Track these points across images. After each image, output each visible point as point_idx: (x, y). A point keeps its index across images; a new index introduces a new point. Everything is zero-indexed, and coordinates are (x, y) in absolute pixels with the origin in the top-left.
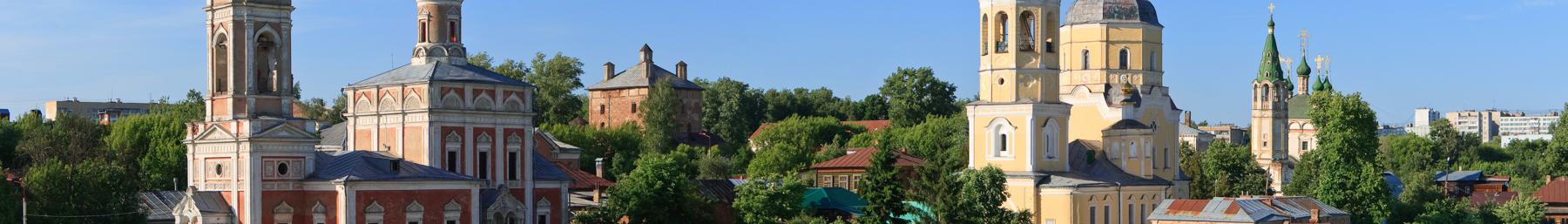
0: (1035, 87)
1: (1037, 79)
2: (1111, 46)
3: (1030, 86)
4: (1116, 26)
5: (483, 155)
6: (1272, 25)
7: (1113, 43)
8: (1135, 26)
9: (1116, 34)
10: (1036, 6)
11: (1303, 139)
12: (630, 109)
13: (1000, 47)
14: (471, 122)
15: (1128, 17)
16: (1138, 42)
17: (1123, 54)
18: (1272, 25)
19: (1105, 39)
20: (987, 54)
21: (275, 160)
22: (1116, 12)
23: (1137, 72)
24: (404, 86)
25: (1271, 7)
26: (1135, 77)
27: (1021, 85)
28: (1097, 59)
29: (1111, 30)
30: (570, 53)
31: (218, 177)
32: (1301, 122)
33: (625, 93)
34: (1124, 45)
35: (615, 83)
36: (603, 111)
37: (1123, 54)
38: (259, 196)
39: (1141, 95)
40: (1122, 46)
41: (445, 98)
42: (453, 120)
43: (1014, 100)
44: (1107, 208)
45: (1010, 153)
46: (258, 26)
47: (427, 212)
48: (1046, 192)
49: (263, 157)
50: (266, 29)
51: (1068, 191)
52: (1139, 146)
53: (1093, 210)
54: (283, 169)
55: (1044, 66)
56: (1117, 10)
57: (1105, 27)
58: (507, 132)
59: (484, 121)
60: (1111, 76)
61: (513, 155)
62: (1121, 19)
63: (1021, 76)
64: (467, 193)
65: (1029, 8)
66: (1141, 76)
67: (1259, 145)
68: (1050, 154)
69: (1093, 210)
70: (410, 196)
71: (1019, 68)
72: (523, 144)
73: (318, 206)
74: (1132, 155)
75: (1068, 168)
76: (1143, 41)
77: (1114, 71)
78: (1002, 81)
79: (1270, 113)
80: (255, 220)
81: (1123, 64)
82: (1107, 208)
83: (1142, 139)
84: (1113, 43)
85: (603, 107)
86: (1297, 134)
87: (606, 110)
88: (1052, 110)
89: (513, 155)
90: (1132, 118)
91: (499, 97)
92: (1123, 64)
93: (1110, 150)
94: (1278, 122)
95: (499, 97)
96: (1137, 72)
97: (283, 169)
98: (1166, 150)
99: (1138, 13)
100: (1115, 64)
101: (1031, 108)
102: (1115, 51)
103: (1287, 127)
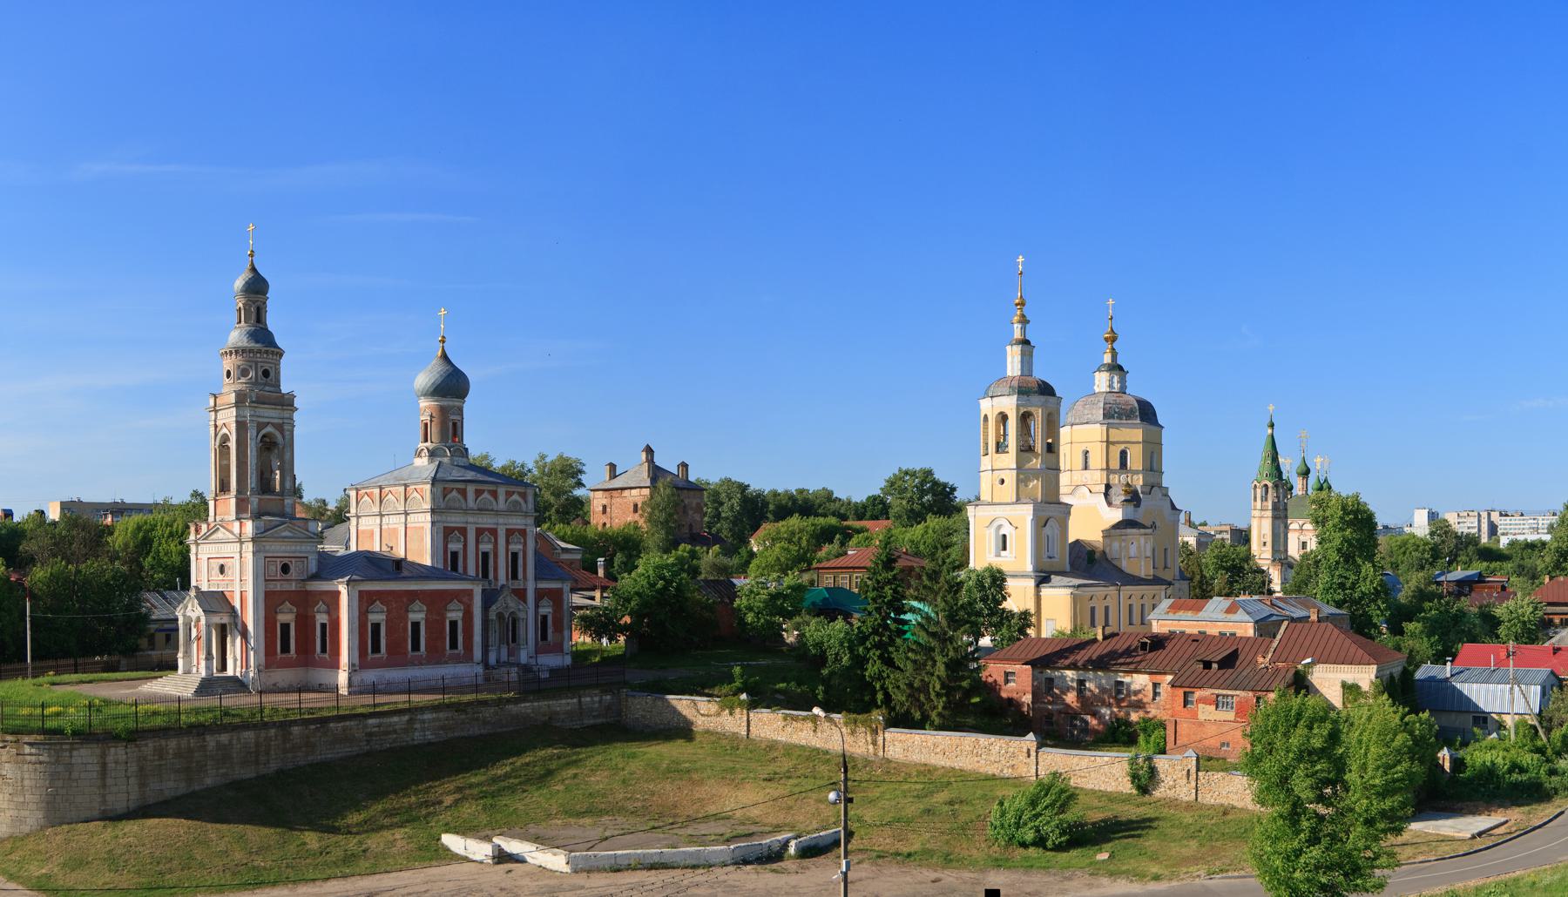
0: (1035, 487)
1: (1038, 480)
2: (1111, 446)
3: (1030, 486)
4: (1117, 427)
5: (485, 555)
6: (1272, 426)
7: (1114, 443)
8: (1134, 426)
9: (1116, 435)
10: (1036, 406)
11: (1303, 539)
12: (632, 509)
13: (1000, 447)
14: (473, 522)
15: (1128, 417)
16: (1138, 443)
17: (1123, 454)
18: (1272, 426)
19: (1105, 439)
20: (987, 454)
21: (278, 560)
22: (1116, 412)
23: (1137, 472)
24: (406, 486)
25: (1271, 408)
26: (1135, 477)
27: (1022, 486)
28: (1097, 460)
29: (1111, 430)
30: (572, 453)
31: (221, 577)
32: (1301, 522)
33: (626, 493)
34: (1125, 445)
35: (617, 483)
36: (604, 511)
37: (1123, 454)
38: (262, 596)
39: (1141, 495)
40: (1122, 447)
41: (446, 499)
42: (455, 520)
43: (1014, 500)
44: (1107, 608)
45: (1011, 553)
46: (260, 426)
47: (429, 612)
48: (1046, 591)
49: (265, 557)
50: (269, 429)
51: (1069, 591)
52: (1139, 547)
53: (1093, 609)
54: (285, 569)
55: (1044, 466)
56: (1117, 410)
57: (1105, 427)
58: (510, 533)
59: (486, 521)
60: (1111, 477)
61: (515, 555)
62: (1121, 419)
63: (1022, 476)
64: (470, 593)
65: (1029, 409)
66: (1141, 476)
67: (1259, 545)
68: (1050, 554)
69: (1093, 609)
70: (413, 596)
71: (1020, 468)
72: (525, 544)
73: (321, 606)
74: (1132, 554)
75: (1068, 568)
76: (1143, 441)
77: (1114, 472)
78: (1002, 482)
79: (1269, 513)
80: (258, 620)
81: (1123, 464)
82: (1107, 608)
83: (1142, 540)
84: (1114, 443)
85: (605, 507)
86: (1297, 534)
87: (608, 510)
88: (1052, 510)
89: (515, 555)
90: (1132, 518)
91: (502, 497)
92: (1123, 464)
93: (1110, 549)
94: (1277, 522)
95: (502, 497)
96: (1137, 472)
97: (285, 569)
98: (1165, 549)
99: (1138, 413)
100: (1115, 464)
101: (1032, 508)
102: (1115, 452)
103: (1286, 527)
